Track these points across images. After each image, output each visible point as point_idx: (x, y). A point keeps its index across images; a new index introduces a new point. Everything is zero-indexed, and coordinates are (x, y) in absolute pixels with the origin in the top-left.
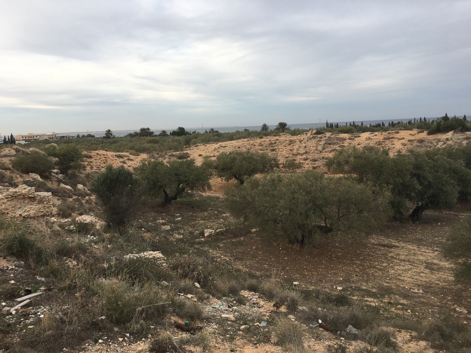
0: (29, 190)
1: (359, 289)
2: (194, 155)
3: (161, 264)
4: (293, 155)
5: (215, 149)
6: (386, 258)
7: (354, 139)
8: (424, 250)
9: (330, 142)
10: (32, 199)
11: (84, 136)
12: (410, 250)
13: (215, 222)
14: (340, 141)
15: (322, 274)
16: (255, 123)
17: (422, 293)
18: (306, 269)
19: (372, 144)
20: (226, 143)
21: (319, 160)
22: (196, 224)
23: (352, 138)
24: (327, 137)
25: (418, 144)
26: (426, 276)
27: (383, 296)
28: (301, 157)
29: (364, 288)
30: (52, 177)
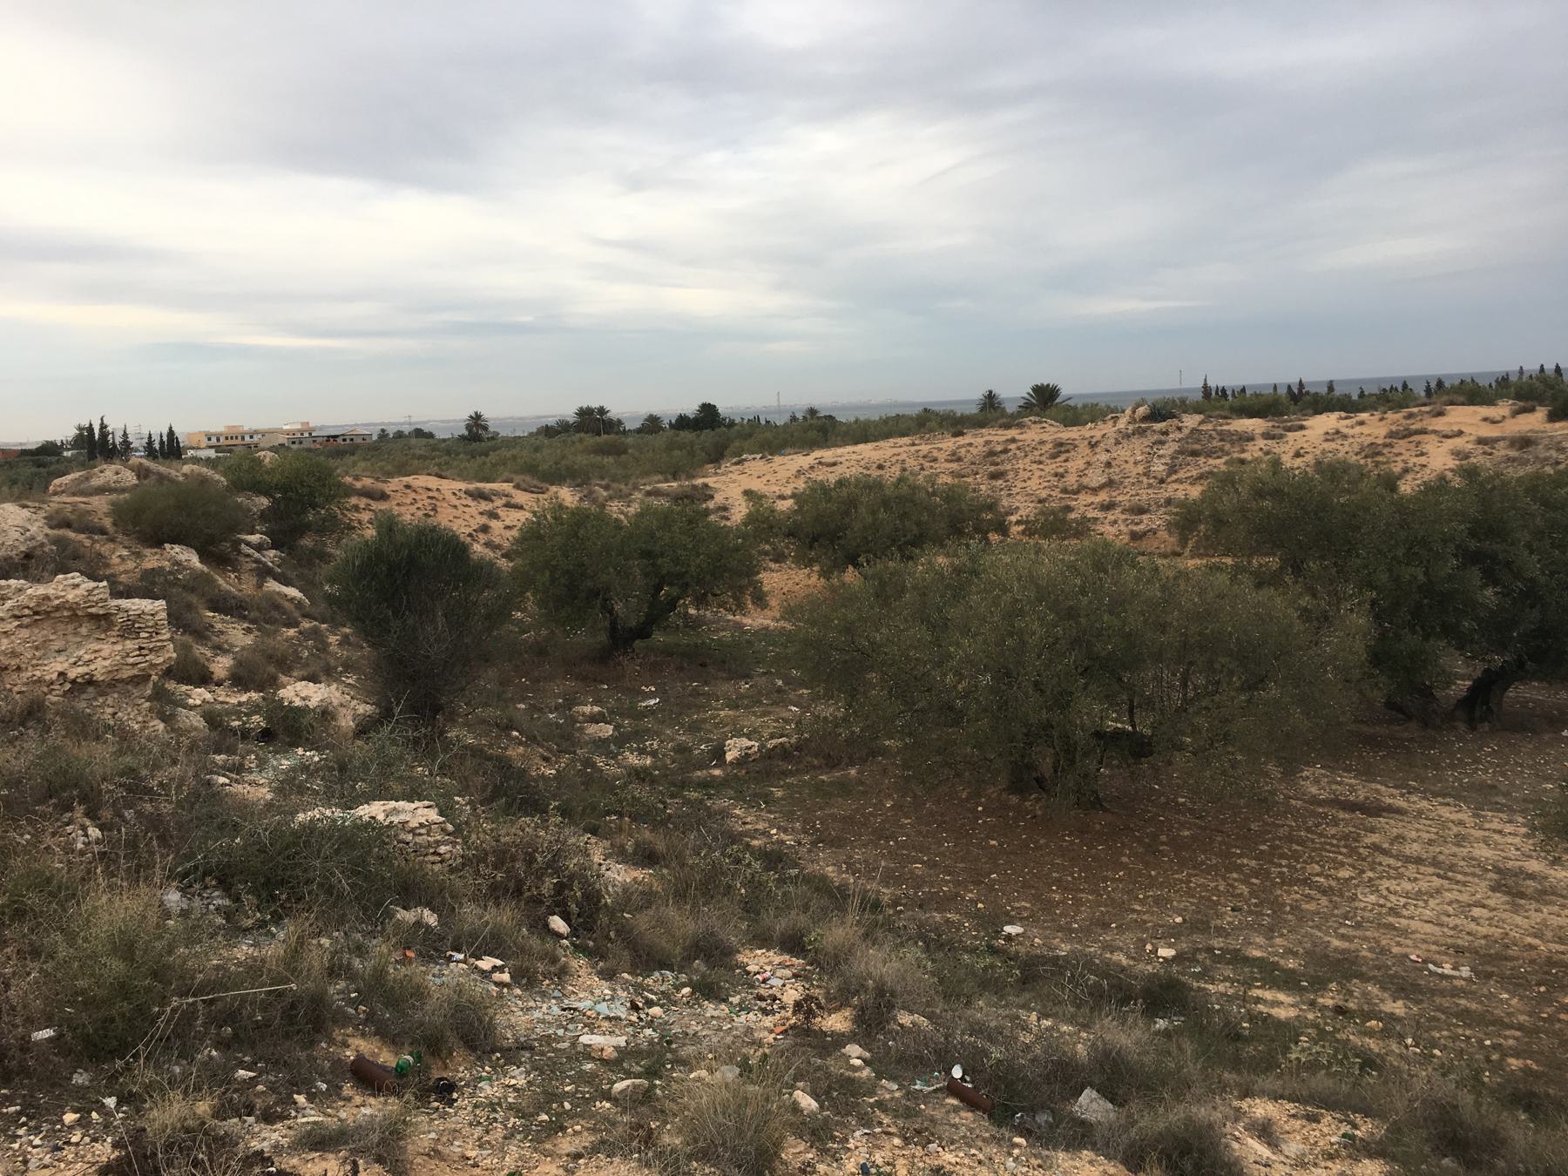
0: (90, 592)
1: (1237, 958)
2: (729, 493)
3: (429, 845)
4: (1065, 491)
5: (799, 473)
6: (1353, 851)
7: (1281, 437)
8: (1495, 825)
9: (1197, 447)
10: (103, 621)
11: (399, 435)
12: (1444, 824)
13: (769, 713)
14: (1233, 443)
15: (1113, 900)
16: (959, 389)
17: (1468, 980)
18: (1058, 881)
19: (1345, 451)
20: (840, 451)
21: (1153, 508)
22: (704, 721)
23: (1277, 431)
24: (1186, 431)
25: (1513, 453)
26: (1495, 919)
27: (1319, 984)
28: (1091, 499)
29: (1257, 953)
30: (242, 559)
